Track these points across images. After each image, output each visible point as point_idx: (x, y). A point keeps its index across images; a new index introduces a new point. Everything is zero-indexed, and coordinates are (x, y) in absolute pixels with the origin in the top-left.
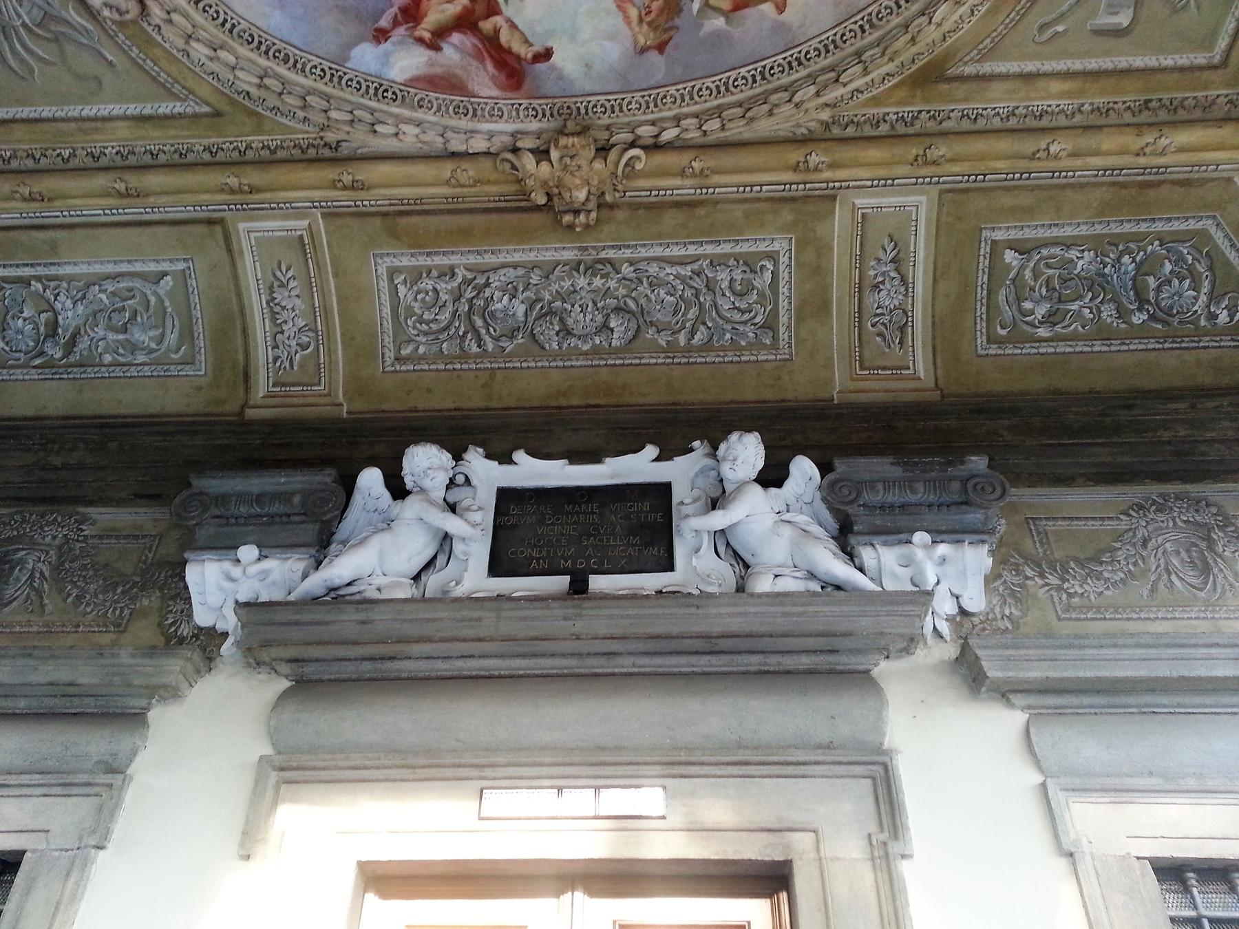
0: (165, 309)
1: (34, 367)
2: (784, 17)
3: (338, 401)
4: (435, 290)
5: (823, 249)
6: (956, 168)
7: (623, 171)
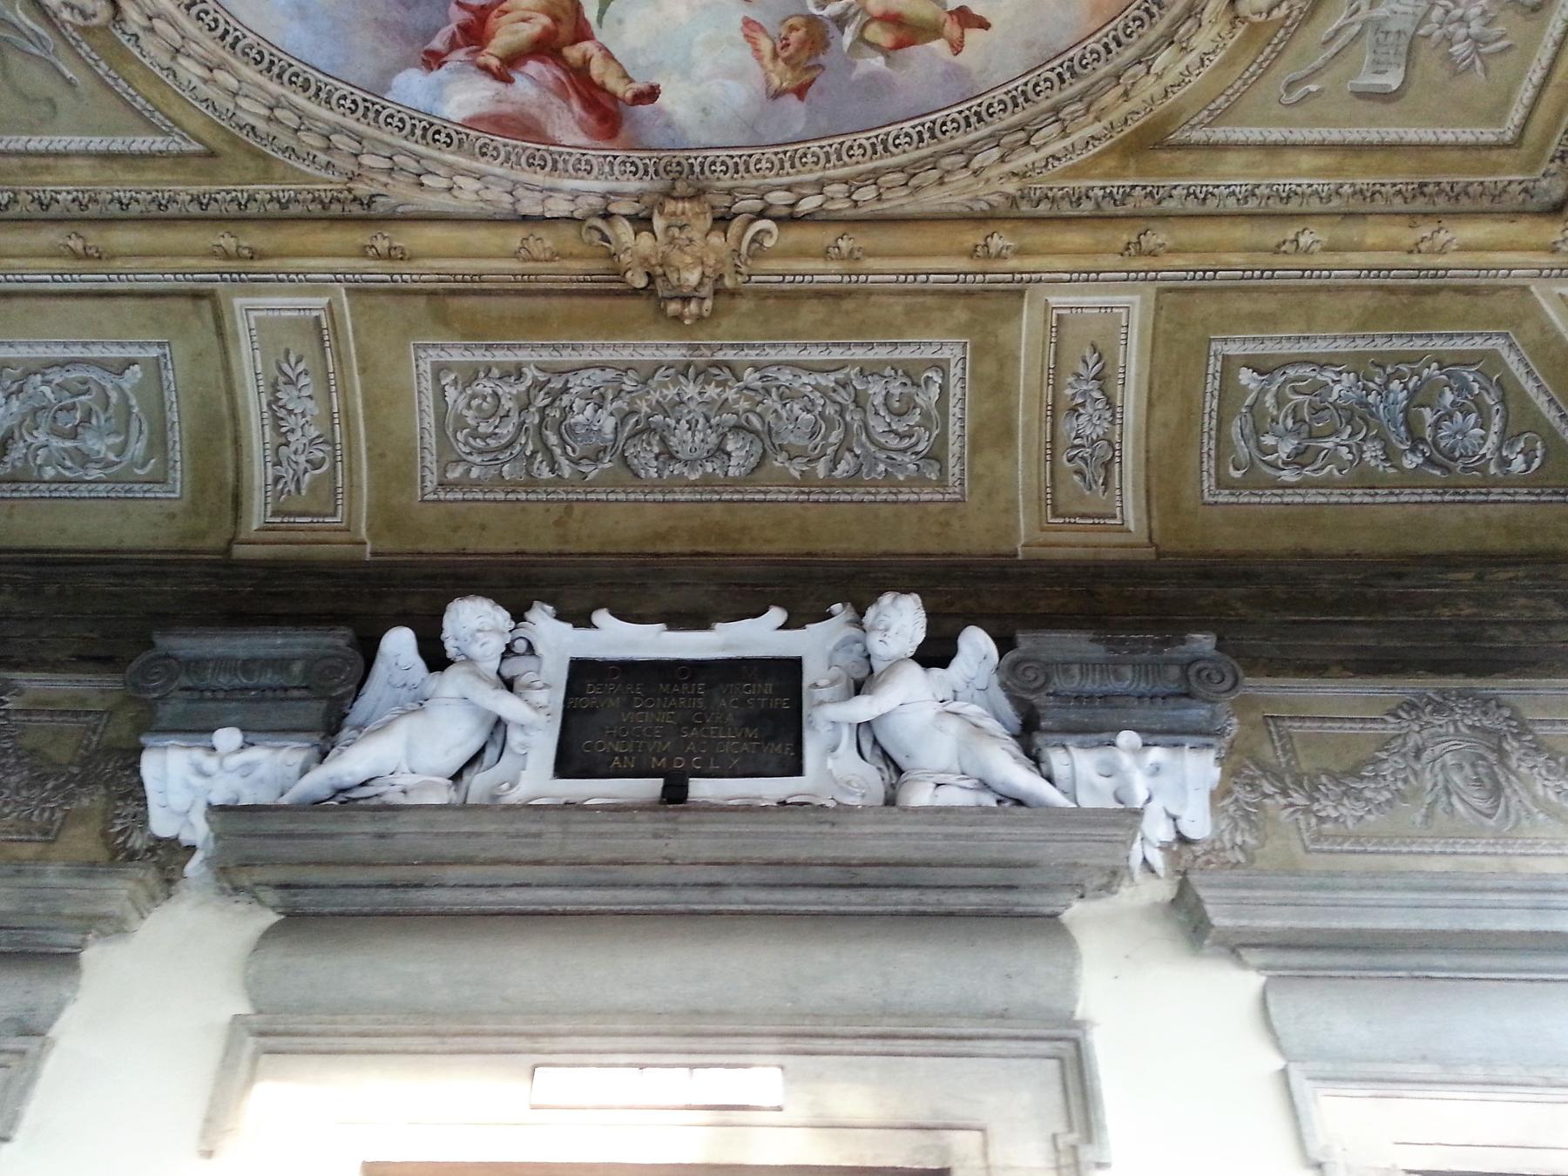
3: (358, 538)
4: (495, 394)
5: (1006, 359)
6: (1179, 262)
7: (749, 247)
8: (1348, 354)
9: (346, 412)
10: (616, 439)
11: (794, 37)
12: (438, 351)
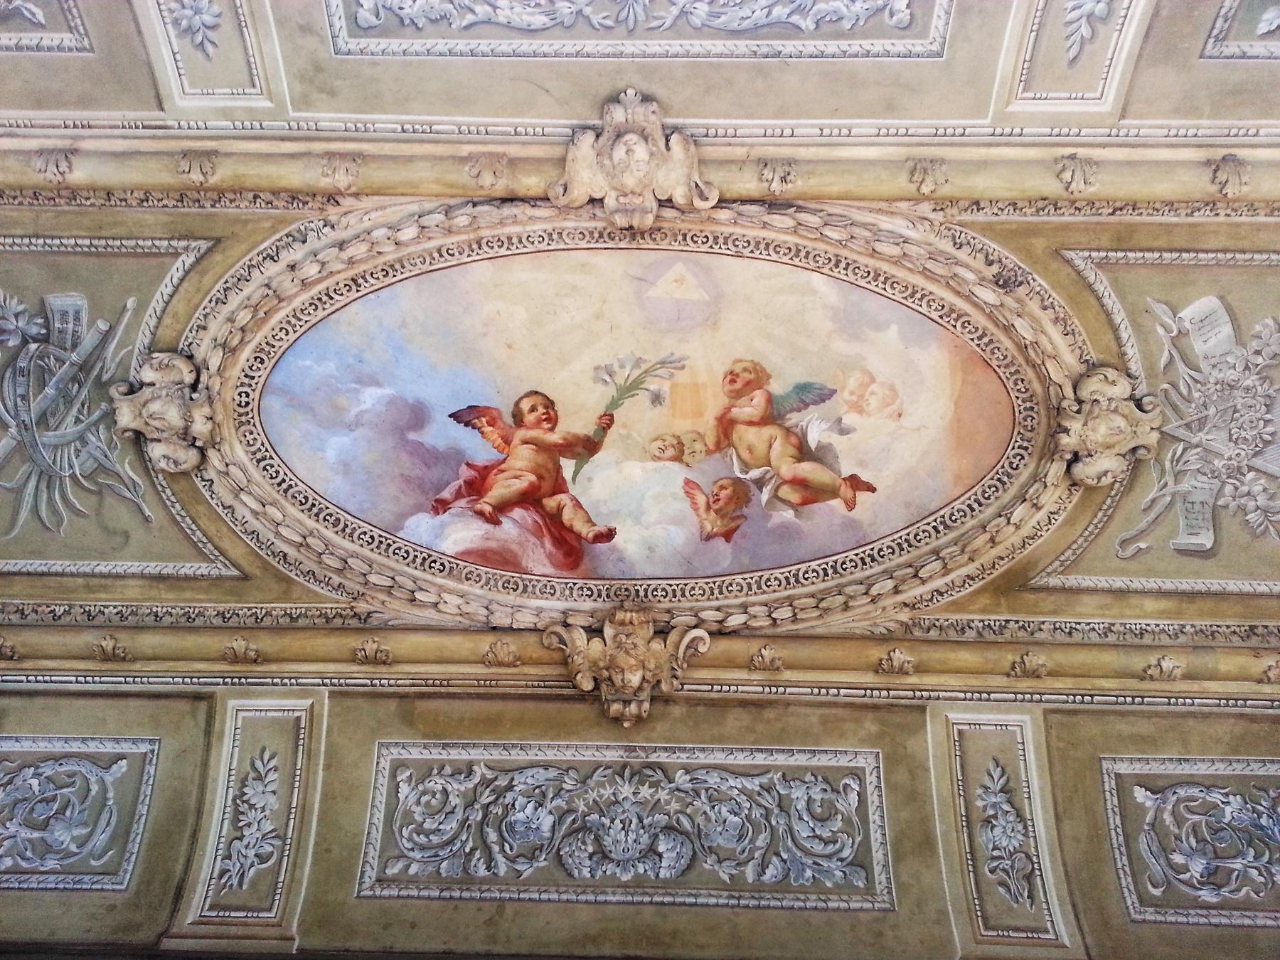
2: (853, 514)
3: (289, 934)
4: (445, 791)
5: (918, 769)
6: (1059, 684)
8: (1229, 777)
9: (304, 808)
10: (552, 838)
11: (724, 494)
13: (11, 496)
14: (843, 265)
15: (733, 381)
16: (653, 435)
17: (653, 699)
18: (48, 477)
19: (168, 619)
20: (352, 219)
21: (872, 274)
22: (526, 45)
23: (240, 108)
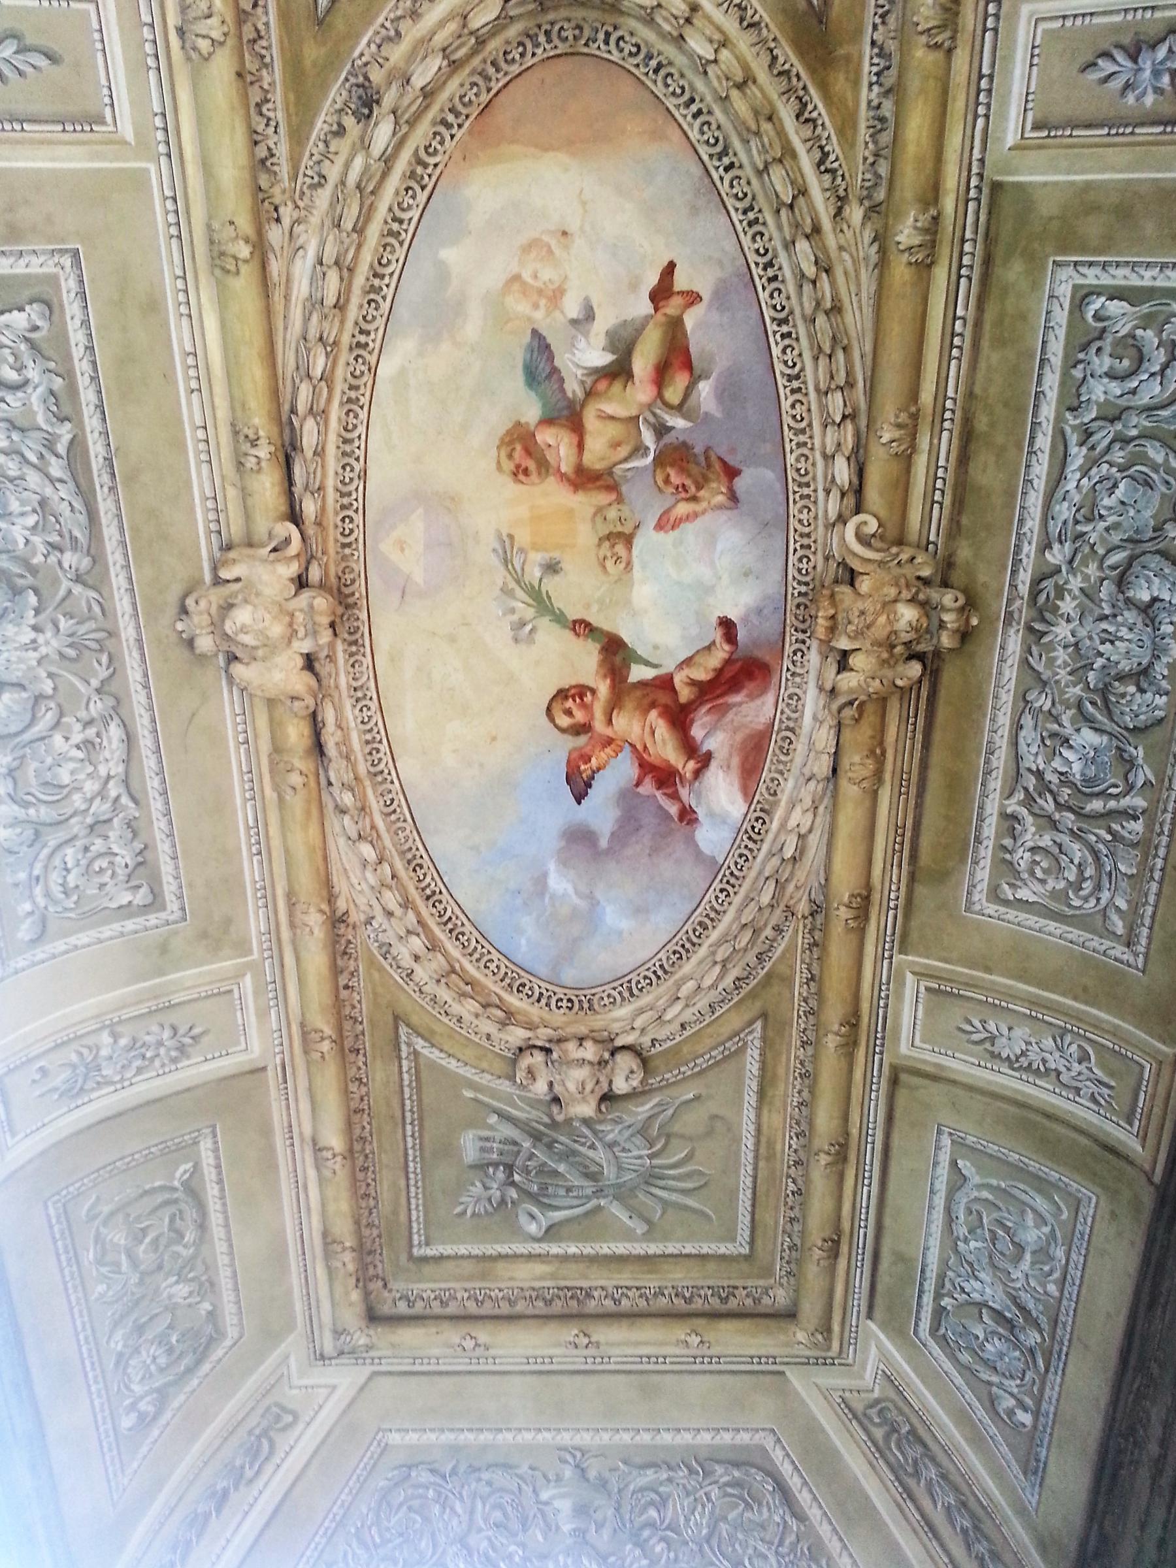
0: (998, 1188)
1: (1047, 1370)
2: (706, 295)
4: (1033, 850)
7: (878, 550)
10: (1110, 734)
11: (675, 479)
12: (976, 891)
13: (670, 1211)
14: (363, 339)
15: (526, 472)
16: (599, 570)
17: (945, 584)
18: (651, 1178)
19: (805, 1094)
20: (361, 901)
21: (372, 296)
22: (145, 742)
23: (255, 1001)
